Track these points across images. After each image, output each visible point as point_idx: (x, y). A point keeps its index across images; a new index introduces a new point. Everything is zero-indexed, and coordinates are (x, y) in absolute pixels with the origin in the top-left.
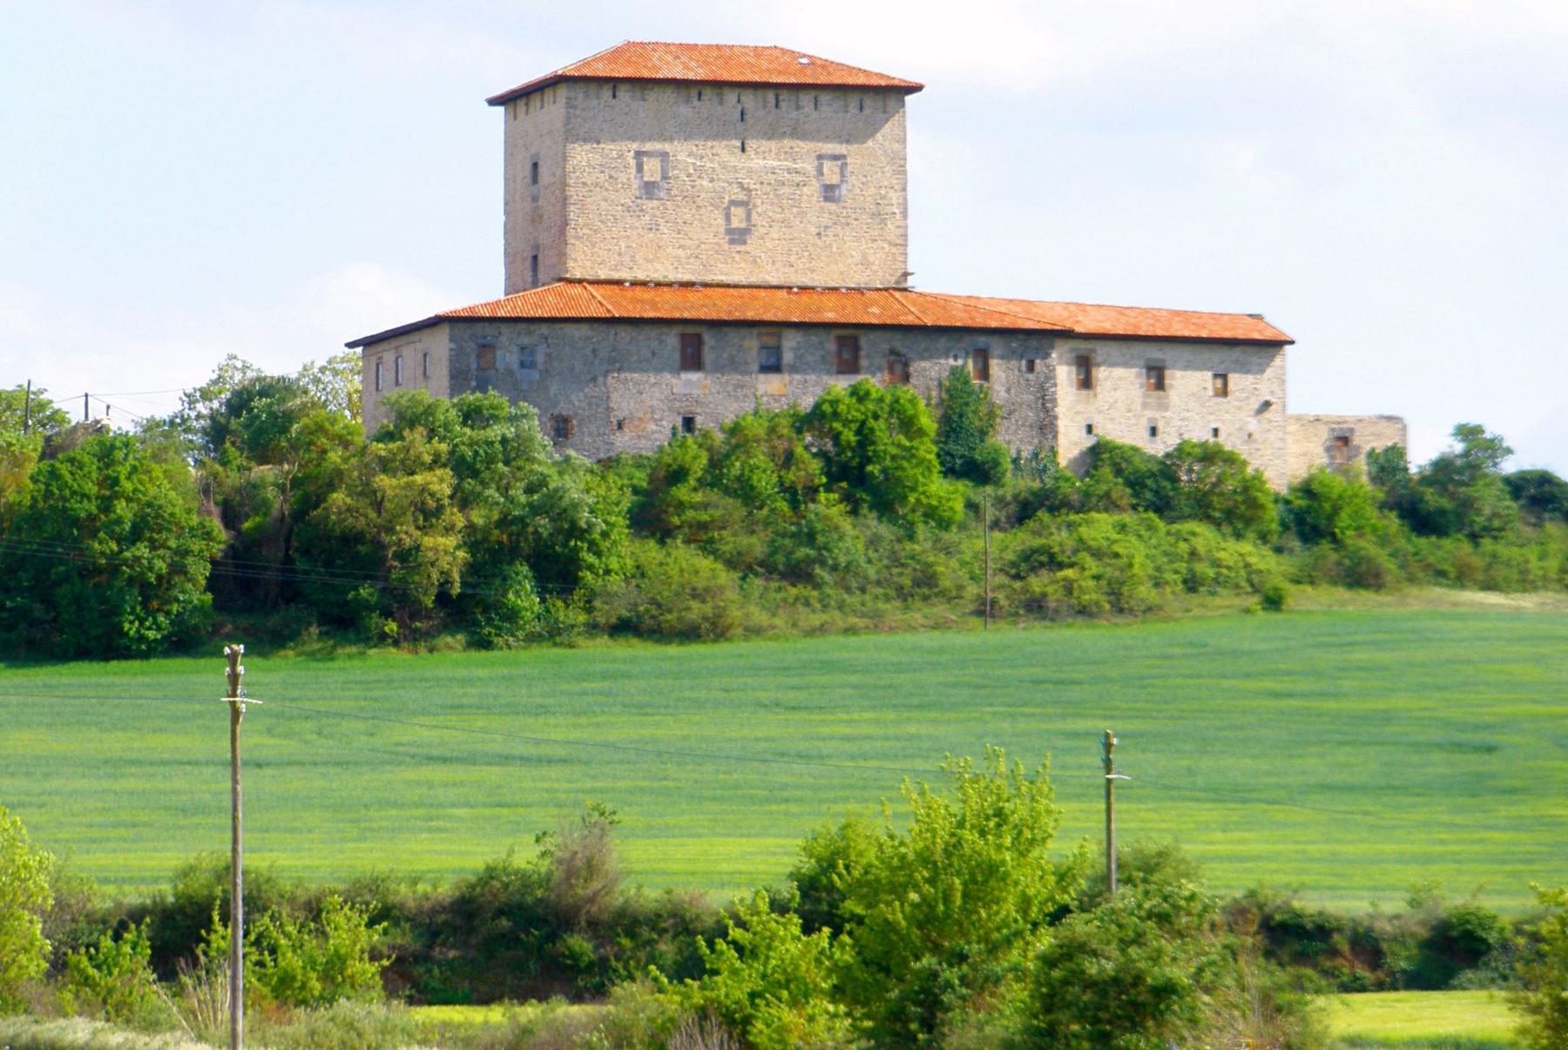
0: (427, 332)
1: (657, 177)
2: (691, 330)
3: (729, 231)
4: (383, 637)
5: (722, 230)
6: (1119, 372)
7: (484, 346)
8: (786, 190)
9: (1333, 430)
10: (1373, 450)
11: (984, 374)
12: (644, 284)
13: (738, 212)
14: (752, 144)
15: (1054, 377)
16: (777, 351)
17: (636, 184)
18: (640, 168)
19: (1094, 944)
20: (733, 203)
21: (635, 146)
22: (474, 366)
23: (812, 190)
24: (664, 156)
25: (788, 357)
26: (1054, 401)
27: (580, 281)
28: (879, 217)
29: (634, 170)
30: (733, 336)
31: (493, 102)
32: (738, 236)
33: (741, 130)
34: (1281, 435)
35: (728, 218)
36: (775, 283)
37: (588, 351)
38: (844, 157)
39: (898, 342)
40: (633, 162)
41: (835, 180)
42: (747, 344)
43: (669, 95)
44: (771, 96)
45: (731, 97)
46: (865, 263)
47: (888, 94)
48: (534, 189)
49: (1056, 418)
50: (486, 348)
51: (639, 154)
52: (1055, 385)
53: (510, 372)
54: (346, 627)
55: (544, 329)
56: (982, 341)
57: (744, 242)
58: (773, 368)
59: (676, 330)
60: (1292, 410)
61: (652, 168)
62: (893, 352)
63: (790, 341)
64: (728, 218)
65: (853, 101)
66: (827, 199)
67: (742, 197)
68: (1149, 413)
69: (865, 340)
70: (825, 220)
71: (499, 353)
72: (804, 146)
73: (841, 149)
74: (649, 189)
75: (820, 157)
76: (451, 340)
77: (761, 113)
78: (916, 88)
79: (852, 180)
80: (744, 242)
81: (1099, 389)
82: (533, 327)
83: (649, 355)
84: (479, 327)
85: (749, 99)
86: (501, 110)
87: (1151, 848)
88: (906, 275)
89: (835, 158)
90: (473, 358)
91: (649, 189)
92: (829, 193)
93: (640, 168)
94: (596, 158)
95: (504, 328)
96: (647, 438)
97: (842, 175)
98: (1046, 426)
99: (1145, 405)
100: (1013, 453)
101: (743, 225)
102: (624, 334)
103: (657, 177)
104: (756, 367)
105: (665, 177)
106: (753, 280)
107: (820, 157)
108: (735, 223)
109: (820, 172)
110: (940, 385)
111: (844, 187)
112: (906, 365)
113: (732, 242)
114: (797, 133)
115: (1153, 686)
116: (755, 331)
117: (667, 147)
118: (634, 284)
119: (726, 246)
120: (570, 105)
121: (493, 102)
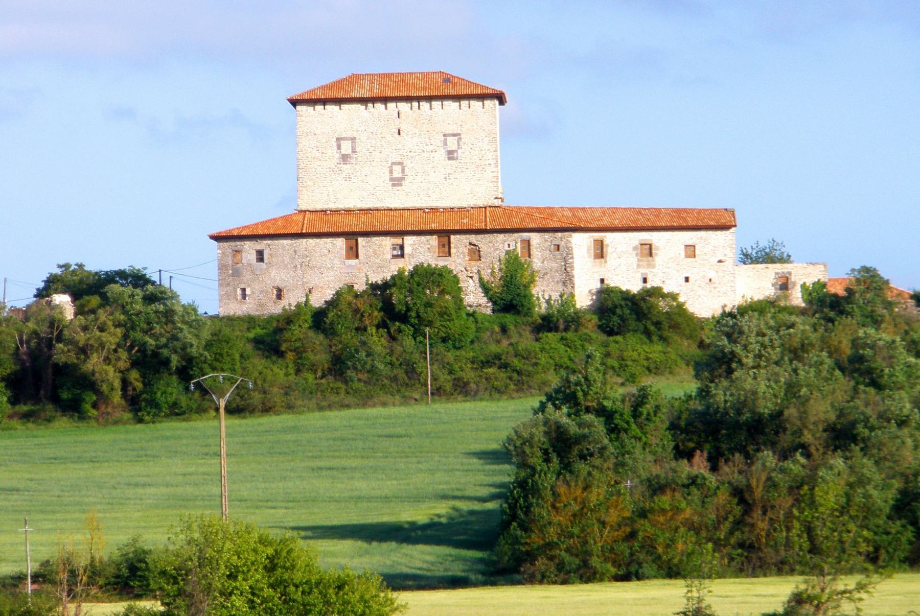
1: (349, 152)
3: (391, 179)
5: (388, 178)
7: (236, 251)
9: (776, 273)
10: (805, 283)
15: (572, 254)
17: (337, 156)
18: (339, 147)
20: (393, 163)
22: (230, 263)
23: (442, 154)
26: (572, 267)
29: (336, 148)
32: (397, 182)
34: (732, 279)
35: (391, 172)
37: (292, 252)
38: (459, 134)
40: (335, 144)
41: (454, 148)
42: (384, 243)
44: (415, 104)
45: (391, 105)
49: (573, 276)
52: (572, 258)
53: (250, 265)
57: (401, 185)
64: (391, 172)
65: (464, 103)
66: (450, 159)
68: (643, 271)
71: (243, 254)
74: (345, 158)
80: (401, 185)
81: (608, 259)
83: (326, 251)
87: (45, 559)
90: (230, 258)
91: (345, 158)
92: (451, 155)
93: (339, 147)
96: (153, 336)
97: (459, 145)
98: (568, 279)
99: (639, 266)
100: (547, 297)
101: (400, 175)
103: (349, 152)
105: (354, 151)
109: (445, 144)
110: (500, 260)
111: (460, 151)
113: (394, 185)
115: (397, 452)
119: (390, 188)
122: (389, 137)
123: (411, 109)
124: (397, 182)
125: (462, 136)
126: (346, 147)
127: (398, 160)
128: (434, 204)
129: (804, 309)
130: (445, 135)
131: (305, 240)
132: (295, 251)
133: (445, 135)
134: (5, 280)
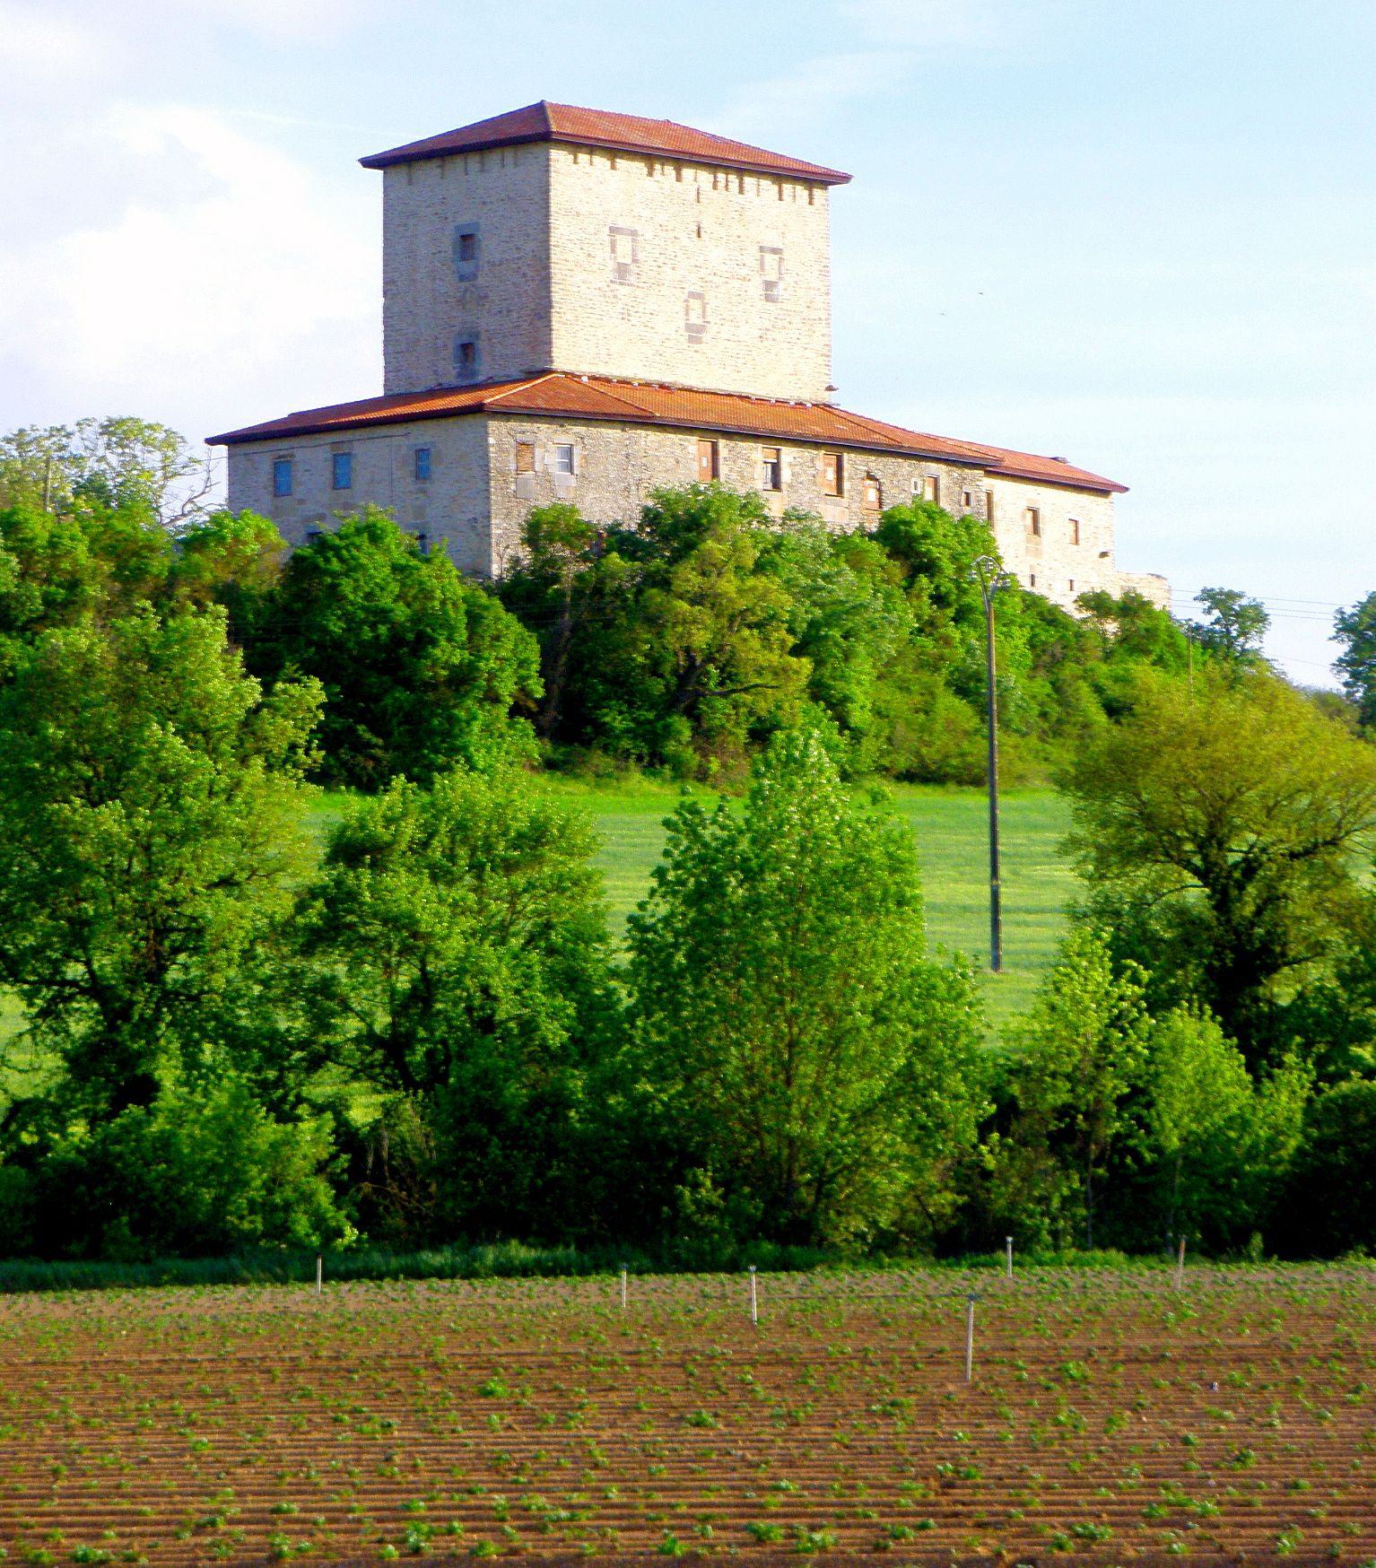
0: (429, 423)
3: (689, 327)
5: (682, 324)
13: (695, 304)
17: (611, 265)
22: (513, 467)
23: (756, 289)
31: (368, 163)
32: (695, 333)
37: (620, 457)
40: (608, 239)
48: (467, 267)
62: (870, 477)
66: (768, 298)
71: (538, 451)
78: (845, 178)
86: (379, 173)
91: (622, 270)
103: (628, 260)
105: (635, 261)
108: (695, 319)
111: (781, 285)
119: (686, 345)
121: (368, 163)
122: (685, 241)
123: (715, 187)
124: (695, 333)
125: (786, 255)
126: (624, 244)
127: (699, 290)
128: (667, 379)
129: (1351, 1042)
130: (762, 249)
131: (643, 433)
132: (627, 456)
133: (762, 249)
134: (1077, 542)
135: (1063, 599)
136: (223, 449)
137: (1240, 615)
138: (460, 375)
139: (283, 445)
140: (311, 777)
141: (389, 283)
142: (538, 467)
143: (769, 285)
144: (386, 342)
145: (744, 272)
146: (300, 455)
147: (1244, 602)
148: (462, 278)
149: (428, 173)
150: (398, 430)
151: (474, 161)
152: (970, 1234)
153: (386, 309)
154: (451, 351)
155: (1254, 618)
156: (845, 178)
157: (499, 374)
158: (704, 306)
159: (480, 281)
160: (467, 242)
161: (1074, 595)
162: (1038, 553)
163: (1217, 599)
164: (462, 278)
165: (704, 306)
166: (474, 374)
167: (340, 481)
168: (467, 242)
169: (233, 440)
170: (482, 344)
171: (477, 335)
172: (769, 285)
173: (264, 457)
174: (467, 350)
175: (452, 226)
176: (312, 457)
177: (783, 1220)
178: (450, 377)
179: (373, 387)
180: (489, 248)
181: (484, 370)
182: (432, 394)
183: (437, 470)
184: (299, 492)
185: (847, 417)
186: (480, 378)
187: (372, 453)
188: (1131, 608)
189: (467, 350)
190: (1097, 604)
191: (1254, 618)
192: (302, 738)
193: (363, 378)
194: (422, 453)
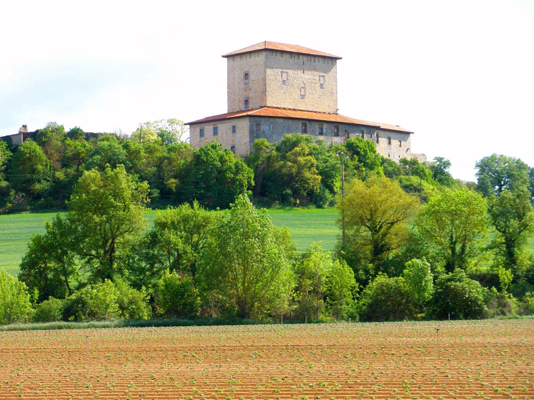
0: (235, 119)
2: (304, 122)
3: (301, 95)
4: (295, 205)
6: (384, 139)
8: (313, 85)
11: (363, 137)
12: (285, 109)
13: (303, 90)
14: (305, 72)
16: (322, 129)
17: (281, 80)
19: (502, 285)
20: (302, 87)
21: (281, 70)
22: (255, 130)
23: (318, 85)
24: (287, 73)
25: (324, 131)
27: (270, 107)
28: (332, 94)
30: (313, 123)
31: (223, 57)
32: (303, 97)
33: (303, 68)
36: (311, 110)
39: (347, 128)
43: (287, 56)
45: (301, 57)
46: (329, 106)
47: (333, 59)
48: (247, 81)
50: (258, 125)
51: (282, 72)
54: (284, 202)
55: (272, 120)
56: (363, 128)
58: (321, 134)
59: (302, 121)
60: (412, 152)
61: (284, 75)
62: (346, 131)
63: (325, 126)
66: (321, 88)
67: (303, 86)
69: (340, 127)
70: (321, 94)
71: (261, 126)
72: (316, 73)
73: (324, 74)
74: (284, 81)
75: (320, 76)
76: (250, 122)
77: (307, 63)
78: (341, 58)
79: (326, 83)
82: (270, 119)
84: (256, 119)
85: (305, 59)
86: (226, 59)
88: (337, 110)
89: (323, 76)
91: (284, 81)
94: (272, 73)
95: (262, 119)
102: (290, 122)
104: (318, 133)
105: (287, 79)
106: (306, 109)
107: (320, 76)
108: (302, 93)
112: (348, 134)
113: (302, 98)
114: (315, 69)
116: (318, 123)
117: (288, 71)
118: (289, 109)
120: (266, 57)
121: (223, 57)
135: (396, 160)
136: (188, 126)
137: (444, 163)
138: (245, 108)
139: (202, 125)
140: (148, 206)
141: (229, 86)
142: (261, 130)
143: (322, 85)
144: (228, 100)
145: (315, 81)
146: (206, 127)
147: (445, 160)
148: (245, 84)
149: (238, 59)
150: (229, 121)
151: (248, 56)
152: (302, 316)
153: (228, 92)
154: (243, 102)
155: (447, 164)
156: (341, 58)
157: (254, 107)
158: (305, 90)
159: (250, 85)
160: (246, 75)
161: (399, 159)
162: (390, 149)
163: (440, 160)
164: (245, 84)
165: (305, 90)
166: (248, 107)
167: (215, 132)
168: (246, 75)
169: (191, 124)
170: (250, 100)
171: (249, 98)
172: (322, 85)
173: (198, 129)
174: (247, 102)
175: (243, 72)
176: (209, 128)
177: (240, 314)
178: (243, 107)
179: (225, 111)
180: (252, 77)
181: (251, 106)
182: (238, 112)
183: (237, 131)
184: (205, 136)
185: (341, 117)
186: (250, 108)
187: (223, 127)
188: (414, 162)
189: (247, 102)
190: (404, 162)
191: (447, 164)
192: (145, 197)
193: (223, 109)
194: (234, 127)
